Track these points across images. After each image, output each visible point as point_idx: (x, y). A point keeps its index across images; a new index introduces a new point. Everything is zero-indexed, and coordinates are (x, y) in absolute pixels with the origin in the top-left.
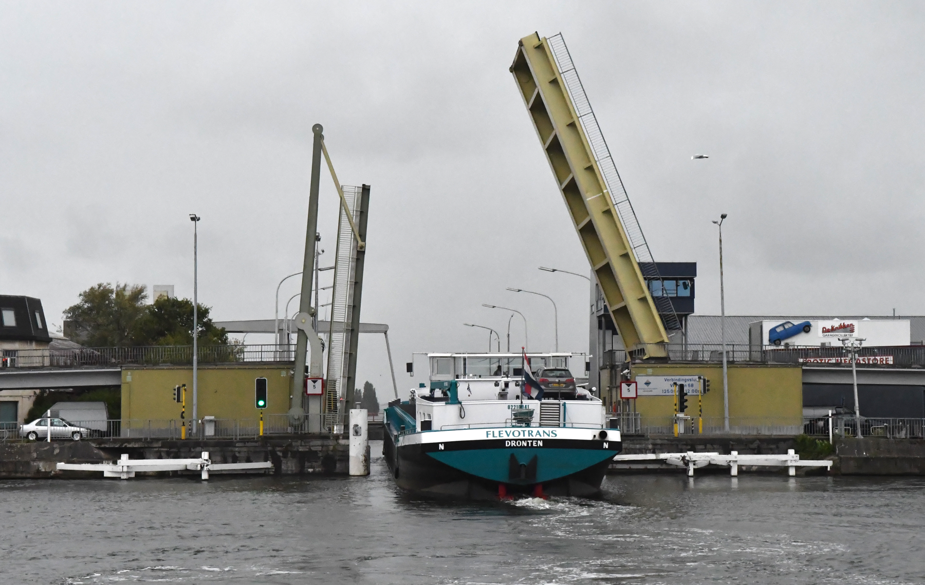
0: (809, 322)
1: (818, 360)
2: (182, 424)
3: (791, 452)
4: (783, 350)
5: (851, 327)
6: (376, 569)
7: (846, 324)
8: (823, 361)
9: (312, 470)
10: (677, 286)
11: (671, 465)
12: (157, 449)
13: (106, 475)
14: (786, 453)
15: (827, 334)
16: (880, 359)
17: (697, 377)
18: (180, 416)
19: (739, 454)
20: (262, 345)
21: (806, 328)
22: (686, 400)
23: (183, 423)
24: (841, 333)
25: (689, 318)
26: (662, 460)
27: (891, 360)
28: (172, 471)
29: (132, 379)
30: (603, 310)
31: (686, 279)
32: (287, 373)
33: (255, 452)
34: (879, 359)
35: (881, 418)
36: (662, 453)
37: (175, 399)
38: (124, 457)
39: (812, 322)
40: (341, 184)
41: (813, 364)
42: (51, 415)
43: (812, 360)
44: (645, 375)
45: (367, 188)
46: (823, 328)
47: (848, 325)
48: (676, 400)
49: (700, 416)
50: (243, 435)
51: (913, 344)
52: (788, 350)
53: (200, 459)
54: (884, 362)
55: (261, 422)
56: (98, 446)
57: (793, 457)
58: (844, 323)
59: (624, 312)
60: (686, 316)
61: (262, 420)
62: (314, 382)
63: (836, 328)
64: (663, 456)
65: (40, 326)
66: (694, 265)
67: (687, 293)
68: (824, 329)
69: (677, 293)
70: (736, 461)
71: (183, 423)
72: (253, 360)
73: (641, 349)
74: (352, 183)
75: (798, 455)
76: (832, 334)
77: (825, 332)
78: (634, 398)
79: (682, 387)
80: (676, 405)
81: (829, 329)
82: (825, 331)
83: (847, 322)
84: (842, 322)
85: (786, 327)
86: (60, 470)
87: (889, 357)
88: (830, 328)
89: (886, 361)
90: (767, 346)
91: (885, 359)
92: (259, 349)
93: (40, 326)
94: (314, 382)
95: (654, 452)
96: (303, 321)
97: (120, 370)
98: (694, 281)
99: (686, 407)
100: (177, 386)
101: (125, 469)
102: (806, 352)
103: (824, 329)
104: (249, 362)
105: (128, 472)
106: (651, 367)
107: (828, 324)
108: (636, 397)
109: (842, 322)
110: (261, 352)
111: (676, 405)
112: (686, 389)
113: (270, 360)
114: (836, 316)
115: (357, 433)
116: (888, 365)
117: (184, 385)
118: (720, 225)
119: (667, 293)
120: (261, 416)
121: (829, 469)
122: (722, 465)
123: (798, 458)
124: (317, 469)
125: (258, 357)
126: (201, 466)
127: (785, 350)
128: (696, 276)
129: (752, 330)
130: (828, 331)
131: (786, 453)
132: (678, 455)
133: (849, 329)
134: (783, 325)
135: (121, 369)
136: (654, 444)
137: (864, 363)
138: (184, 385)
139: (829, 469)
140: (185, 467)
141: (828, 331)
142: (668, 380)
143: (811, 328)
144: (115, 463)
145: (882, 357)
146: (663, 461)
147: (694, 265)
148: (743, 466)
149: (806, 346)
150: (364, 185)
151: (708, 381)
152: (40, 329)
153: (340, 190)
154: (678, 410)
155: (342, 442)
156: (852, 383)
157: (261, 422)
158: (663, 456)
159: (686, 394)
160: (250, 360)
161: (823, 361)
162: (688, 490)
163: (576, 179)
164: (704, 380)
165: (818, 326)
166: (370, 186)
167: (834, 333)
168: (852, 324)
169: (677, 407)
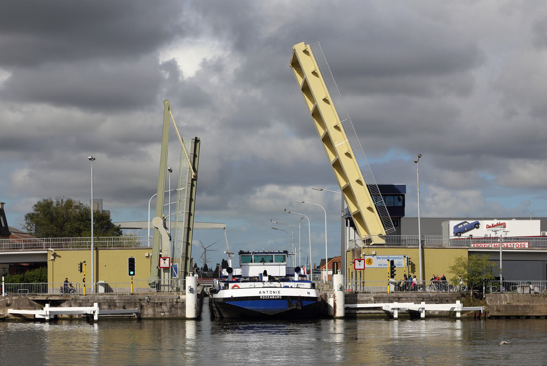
2: (131, 283)
3: (458, 302)
6: (484, 356)
9: (163, 314)
15: (489, 229)
16: (520, 244)
18: (82, 280)
21: (476, 226)
22: (395, 271)
23: (85, 285)
25: (401, 218)
30: (348, 214)
33: (129, 303)
34: (519, 245)
38: (47, 305)
39: (480, 222)
41: (484, 248)
48: (389, 270)
58: (500, 222)
59: (358, 215)
60: (400, 218)
62: (165, 260)
65: (3, 225)
68: (488, 226)
69: (394, 204)
71: (85, 285)
73: (368, 239)
78: (363, 269)
79: (392, 262)
80: (389, 273)
81: (490, 226)
82: (488, 227)
83: (502, 222)
84: (498, 221)
88: (491, 225)
91: (519, 245)
93: (3, 225)
94: (165, 260)
96: (157, 222)
99: (395, 275)
103: (488, 226)
108: (364, 269)
111: (389, 273)
112: (395, 263)
114: (514, 217)
115: (358, 285)
117: (85, 262)
124: (166, 313)
126: (93, 311)
130: (490, 227)
133: (502, 226)
136: (375, 298)
137: (510, 247)
138: (85, 262)
141: (490, 227)
142: (379, 258)
144: (42, 309)
145: (521, 243)
146: (380, 308)
148: (430, 311)
149: (465, 237)
151: (410, 259)
152: (3, 227)
154: (390, 277)
159: (395, 267)
161: (486, 246)
162: (319, 329)
163: (328, 133)
164: (407, 258)
169: (390, 275)
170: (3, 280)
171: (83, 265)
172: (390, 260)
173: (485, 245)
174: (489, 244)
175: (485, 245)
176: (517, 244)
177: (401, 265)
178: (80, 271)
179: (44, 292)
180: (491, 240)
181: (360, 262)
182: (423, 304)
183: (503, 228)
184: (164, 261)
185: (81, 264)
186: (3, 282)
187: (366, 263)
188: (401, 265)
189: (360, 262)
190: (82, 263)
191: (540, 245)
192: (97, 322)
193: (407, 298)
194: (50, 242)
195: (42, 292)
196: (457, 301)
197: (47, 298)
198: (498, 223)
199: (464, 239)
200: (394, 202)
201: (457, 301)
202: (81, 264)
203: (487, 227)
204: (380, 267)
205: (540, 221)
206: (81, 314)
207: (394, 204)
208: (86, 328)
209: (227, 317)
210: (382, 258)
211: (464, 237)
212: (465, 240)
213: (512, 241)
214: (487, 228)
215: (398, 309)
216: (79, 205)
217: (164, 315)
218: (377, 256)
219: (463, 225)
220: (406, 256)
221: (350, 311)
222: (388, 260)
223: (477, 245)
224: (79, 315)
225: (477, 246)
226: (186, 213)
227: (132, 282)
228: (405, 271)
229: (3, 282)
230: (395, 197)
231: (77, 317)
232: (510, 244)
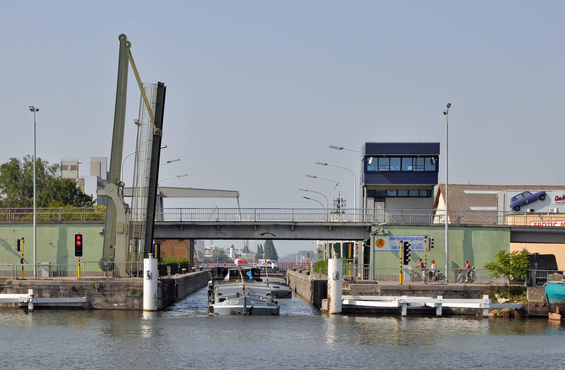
0: (544, 192)
8: (550, 225)
9: (117, 304)
15: (559, 201)
20: (181, 209)
31: (431, 156)
40: (143, 81)
45: (161, 85)
53: (27, 295)
67: (433, 168)
68: (557, 198)
69: (424, 168)
74: (150, 83)
76: (563, 201)
80: (401, 258)
81: (560, 198)
82: (558, 199)
88: (562, 197)
90: (508, 213)
96: (111, 190)
98: (438, 157)
103: (557, 198)
111: (401, 258)
119: (416, 168)
125: (195, 218)
128: (439, 154)
130: (560, 199)
138: (23, 238)
140: (424, 304)
143: (546, 196)
150: (159, 83)
151: (433, 240)
153: (141, 85)
164: (430, 240)
166: (164, 84)
171: (21, 242)
172: (404, 242)
177: (422, 248)
178: (17, 250)
185: (19, 241)
187: (376, 245)
188: (422, 248)
190: (20, 240)
192: (33, 311)
200: (424, 166)
202: (19, 241)
203: (556, 199)
206: (18, 303)
207: (424, 168)
208: (474, 325)
210: (396, 239)
215: (408, 304)
216: (76, 164)
217: (119, 306)
218: (391, 236)
220: (428, 237)
222: (402, 242)
223: (538, 223)
224: (16, 304)
225: (539, 224)
226: (147, 178)
227: (79, 264)
228: (426, 256)
230: (391, 158)
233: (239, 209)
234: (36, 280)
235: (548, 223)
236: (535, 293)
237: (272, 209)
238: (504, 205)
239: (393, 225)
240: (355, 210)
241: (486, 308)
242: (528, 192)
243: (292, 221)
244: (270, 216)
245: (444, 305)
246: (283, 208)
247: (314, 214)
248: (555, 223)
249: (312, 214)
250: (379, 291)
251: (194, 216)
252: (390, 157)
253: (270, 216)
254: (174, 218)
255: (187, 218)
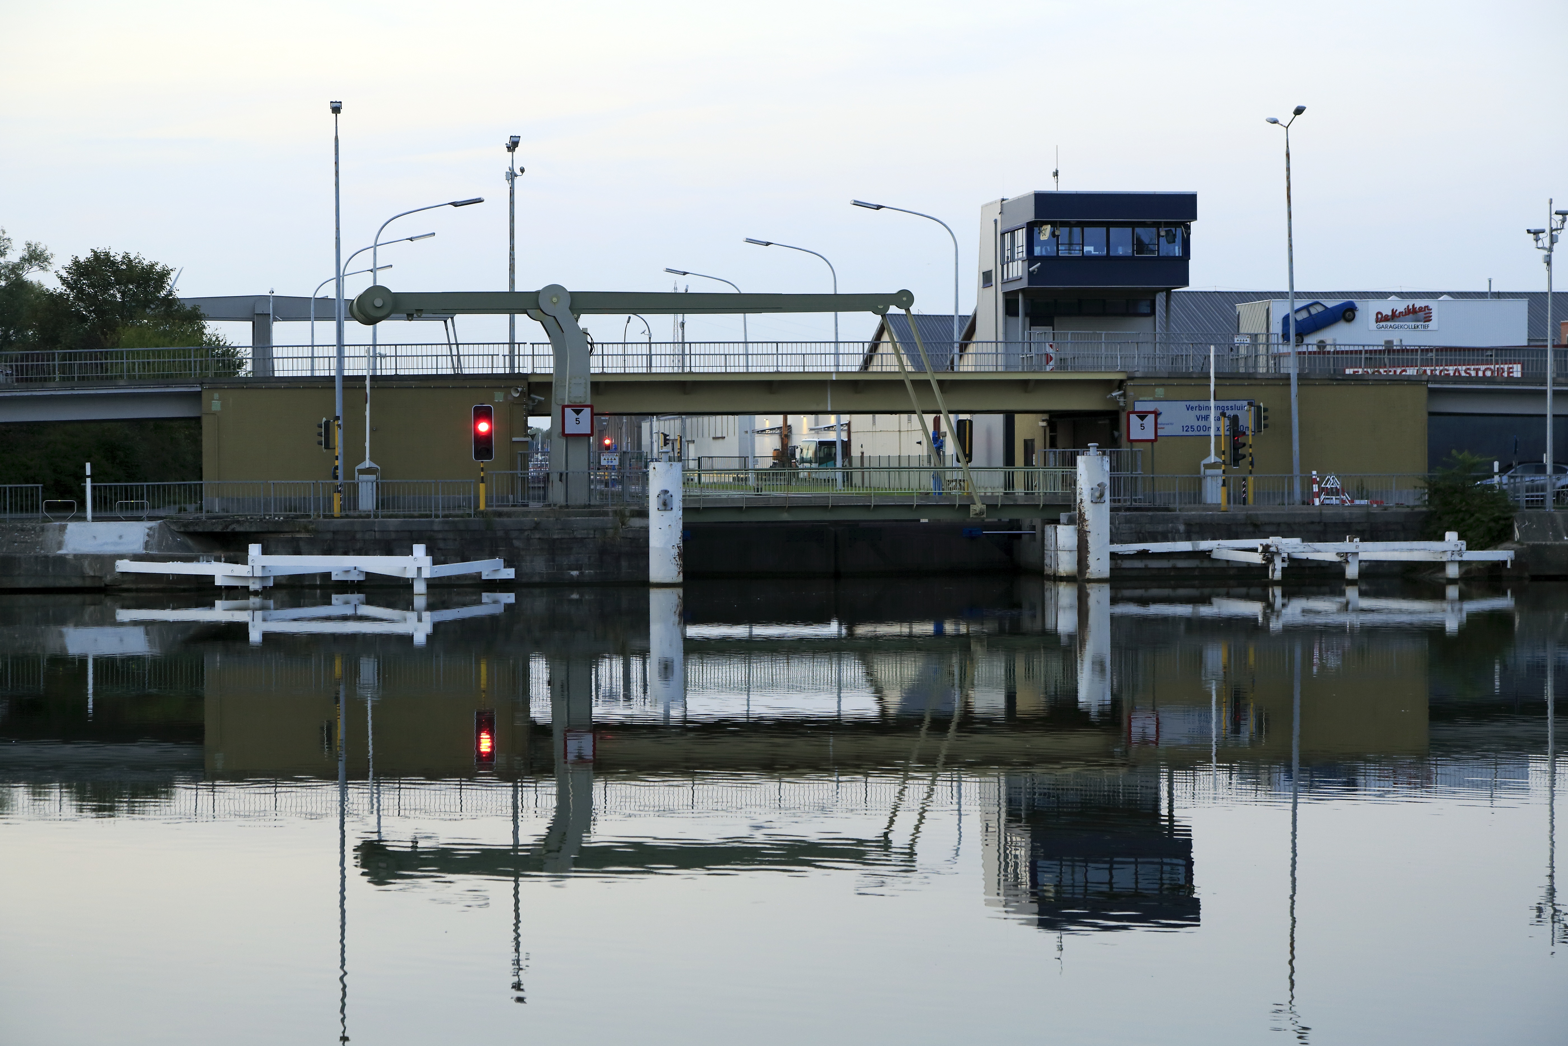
0: (1352, 304)
1: (1382, 370)
4: (1315, 353)
5: (1427, 311)
7: (1417, 306)
10: (1159, 236)
11: (1219, 560)
12: (289, 536)
13: (218, 583)
14: (1442, 538)
15: (1384, 324)
17: (1245, 403)
19: (1361, 541)
24: (1408, 323)
26: (1203, 552)
27: (1517, 371)
28: (172, 574)
29: (222, 406)
32: (505, 397)
34: (1506, 369)
35: (159, 483)
36: (1203, 539)
37: (320, 443)
39: (1358, 303)
42: (1499, 470)
43: (1398, 371)
44: (1151, 398)
46: (1378, 314)
47: (1421, 309)
49: (1251, 472)
50: (454, 508)
51: (1532, 344)
52: (1324, 353)
54: (1505, 375)
55: (482, 486)
56: (182, 530)
57: (1456, 545)
61: (483, 482)
62: (578, 412)
63: (1400, 313)
64: (1204, 545)
66: (1191, 199)
68: (1380, 316)
70: (1357, 553)
72: (411, 372)
75: (1465, 543)
76: (1392, 324)
77: (1381, 321)
82: (1381, 318)
83: (1419, 303)
84: (1410, 302)
85: (1313, 311)
86: (123, 573)
87: (1515, 366)
88: (1390, 314)
89: (1509, 373)
91: (1506, 369)
92: (772, 348)
94: (578, 412)
95: (1188, 538)
97: (200, 389)
98: (1189, 227)
100: (324, 419)
101: (258, 573)
102: (1353, 356)
103: (1380, 316)
104: (418, 375)
105: (262, 578)
106: (1163, 385)
107: (1386, 307)
108: (1156, 440)
109: (1410, 302)
110: (777, 354)
113: (304, 375)
116: (1511, 380)
118: (1287, 127)
120: (482, 474)
121: (1509, 566)
122: (1324, 561)
123: (1464, 547)
125: (823, 364)
127: (1319, 353)
128: (1195, 218)
129: (560, 331)
130: (1386, 319)
131: (1442, 538)
132: (1256, 543)
133: (1422, 314)
134: (1307, 308)
135: (202, 388)
139: (1509, 566)
141: (1386, 319)
142: (1192, 408)
143: (1357, 314)
146: (1205, 555)
147: (1191, 199)
149: (1364, 346)
155: (636, 522)
156: (1544, 413)
157: (482, 486)
158: (1204, 545)
160: (407, 372)
165: (1368, 310)
167: (1397, 323)
168: (1427, 306)
170: (88, 472)
173: (1477, 370)
174: (1441, 368)
175: (1477, 370)
176: (1488, 368)
179: (16, 511)
180: (1384, 354)
181: (578, 415)
182: (1347, 546)
183: (1422, 323)
184: (1142, 422)
186: (88, 480)
189: (578, 415)
191: (1541, 370)
193: (1279, 524)
194: (190, 357)
195: (11, 511)
196: (415, 546)
197: (227, 527)
198: (1408, 306)
199: (1361, 352)
201: (415, 546)
204: (1185, 433)
205: (1527, 303)
209: (1088, 583)
211: (1361, 348)
212: (1331, 356)
213: (1502, 360)
214: (1377, 321)
219: (1309, 312)
221: (1119, 561)
229: (88, 480)
231: (318, 583)
232: (1511, 368)
233: (625, 343)
234: (376, 516)
235: (1474, 369)
236: (1532, 525)
237: (811, 342)
238: (447, 329)
239: (386, 388)
240: (1276, 346)
241: (1452, 561)
242: (1317, 303)
243: (601, 370)
244: (816, 359)
245: (1363, 556)
246: (1371, 343)
247: (739, 355)
248: (1486, 369)
249: (734, 355)
250: (1182, 528)
251: (731, 360)
252: (1108, 225)
253: (816, 359)
254: (547, 366)
255: (790, 365)
